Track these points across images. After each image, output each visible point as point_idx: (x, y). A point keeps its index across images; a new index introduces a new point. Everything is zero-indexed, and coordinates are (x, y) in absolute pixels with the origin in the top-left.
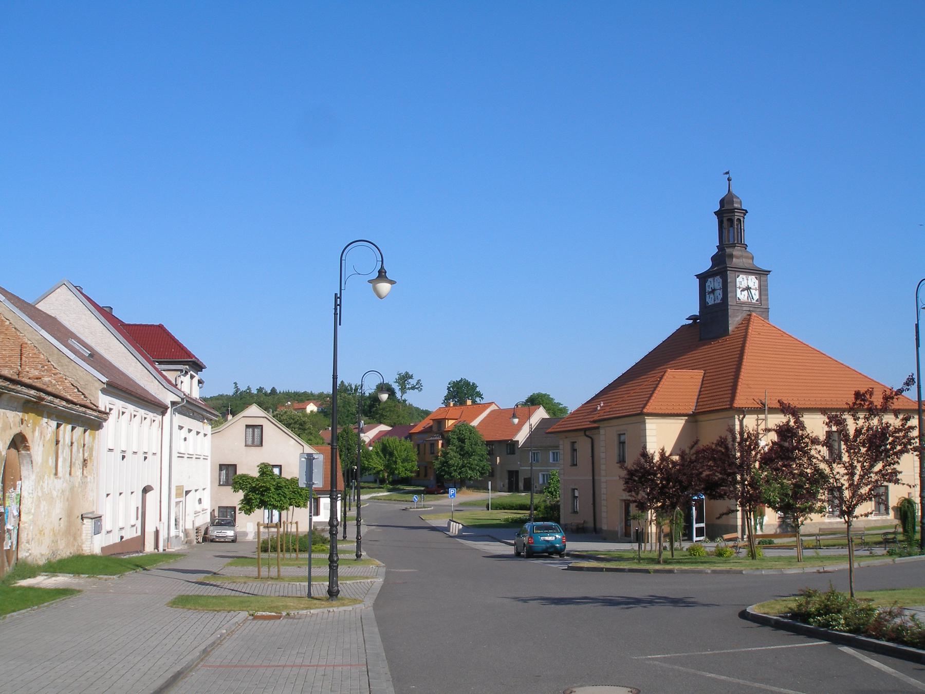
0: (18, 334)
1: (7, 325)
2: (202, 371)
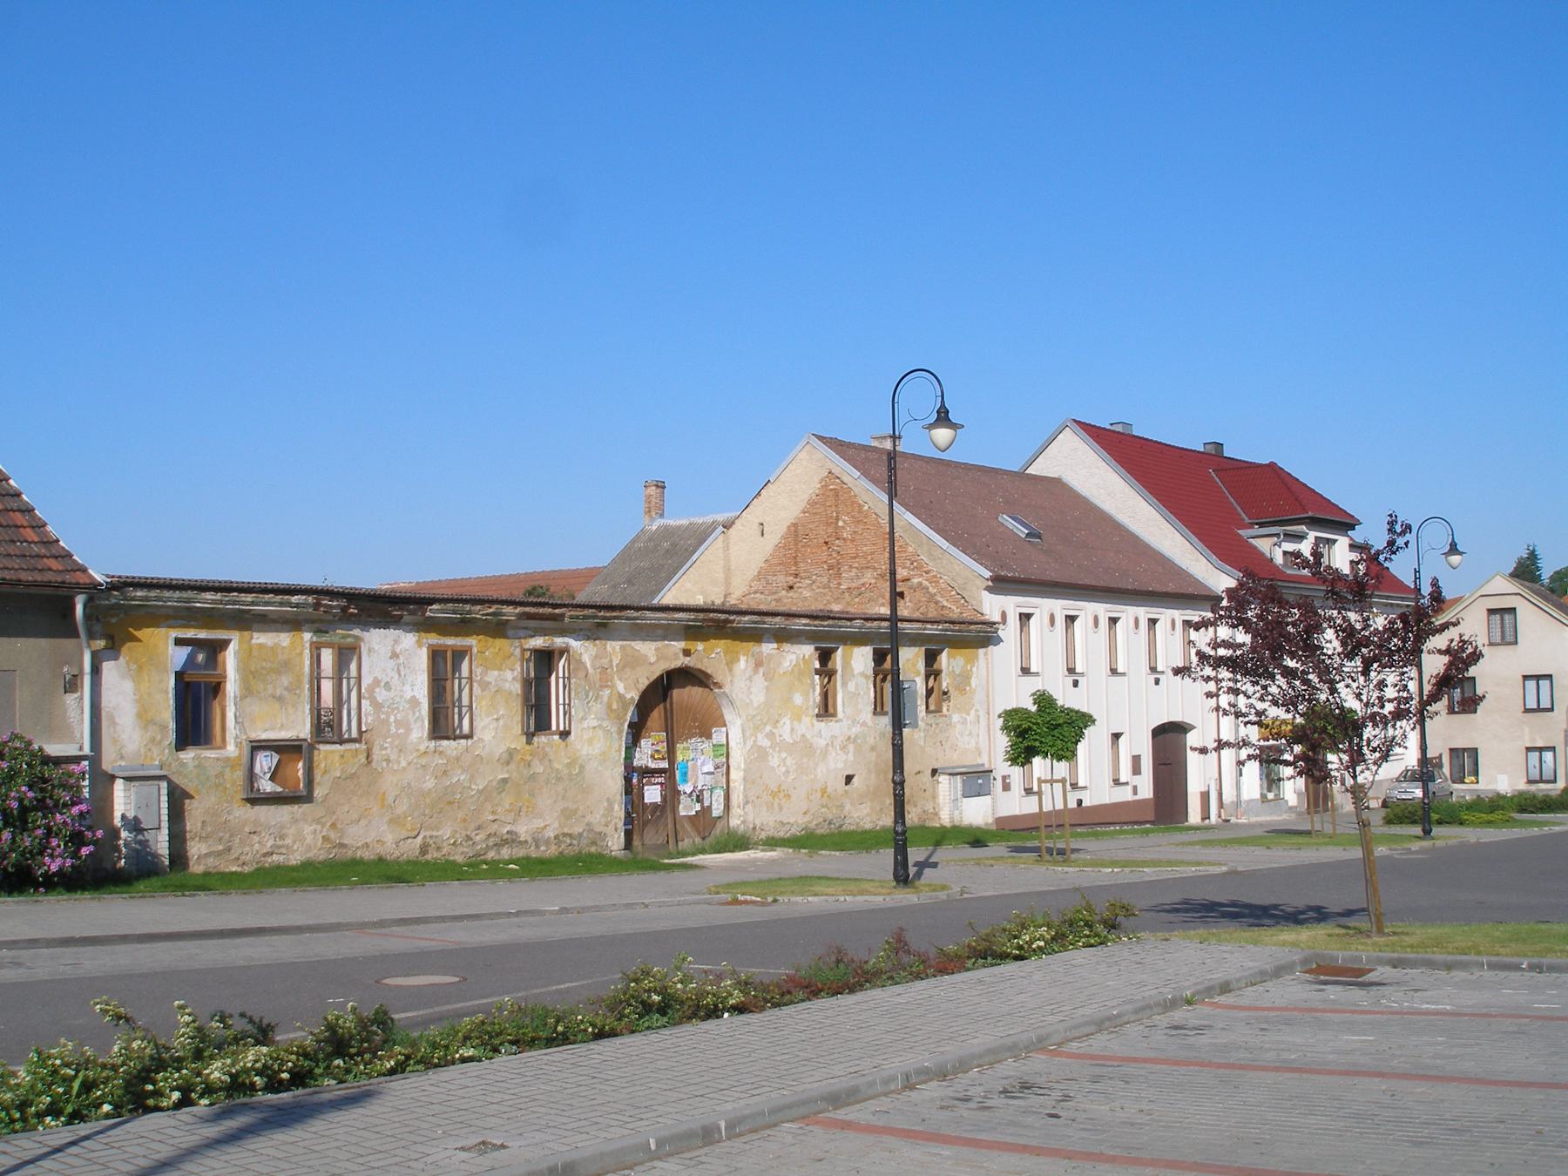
0: (880, 520)
1: (866, 511)
2: (1354, 529)
